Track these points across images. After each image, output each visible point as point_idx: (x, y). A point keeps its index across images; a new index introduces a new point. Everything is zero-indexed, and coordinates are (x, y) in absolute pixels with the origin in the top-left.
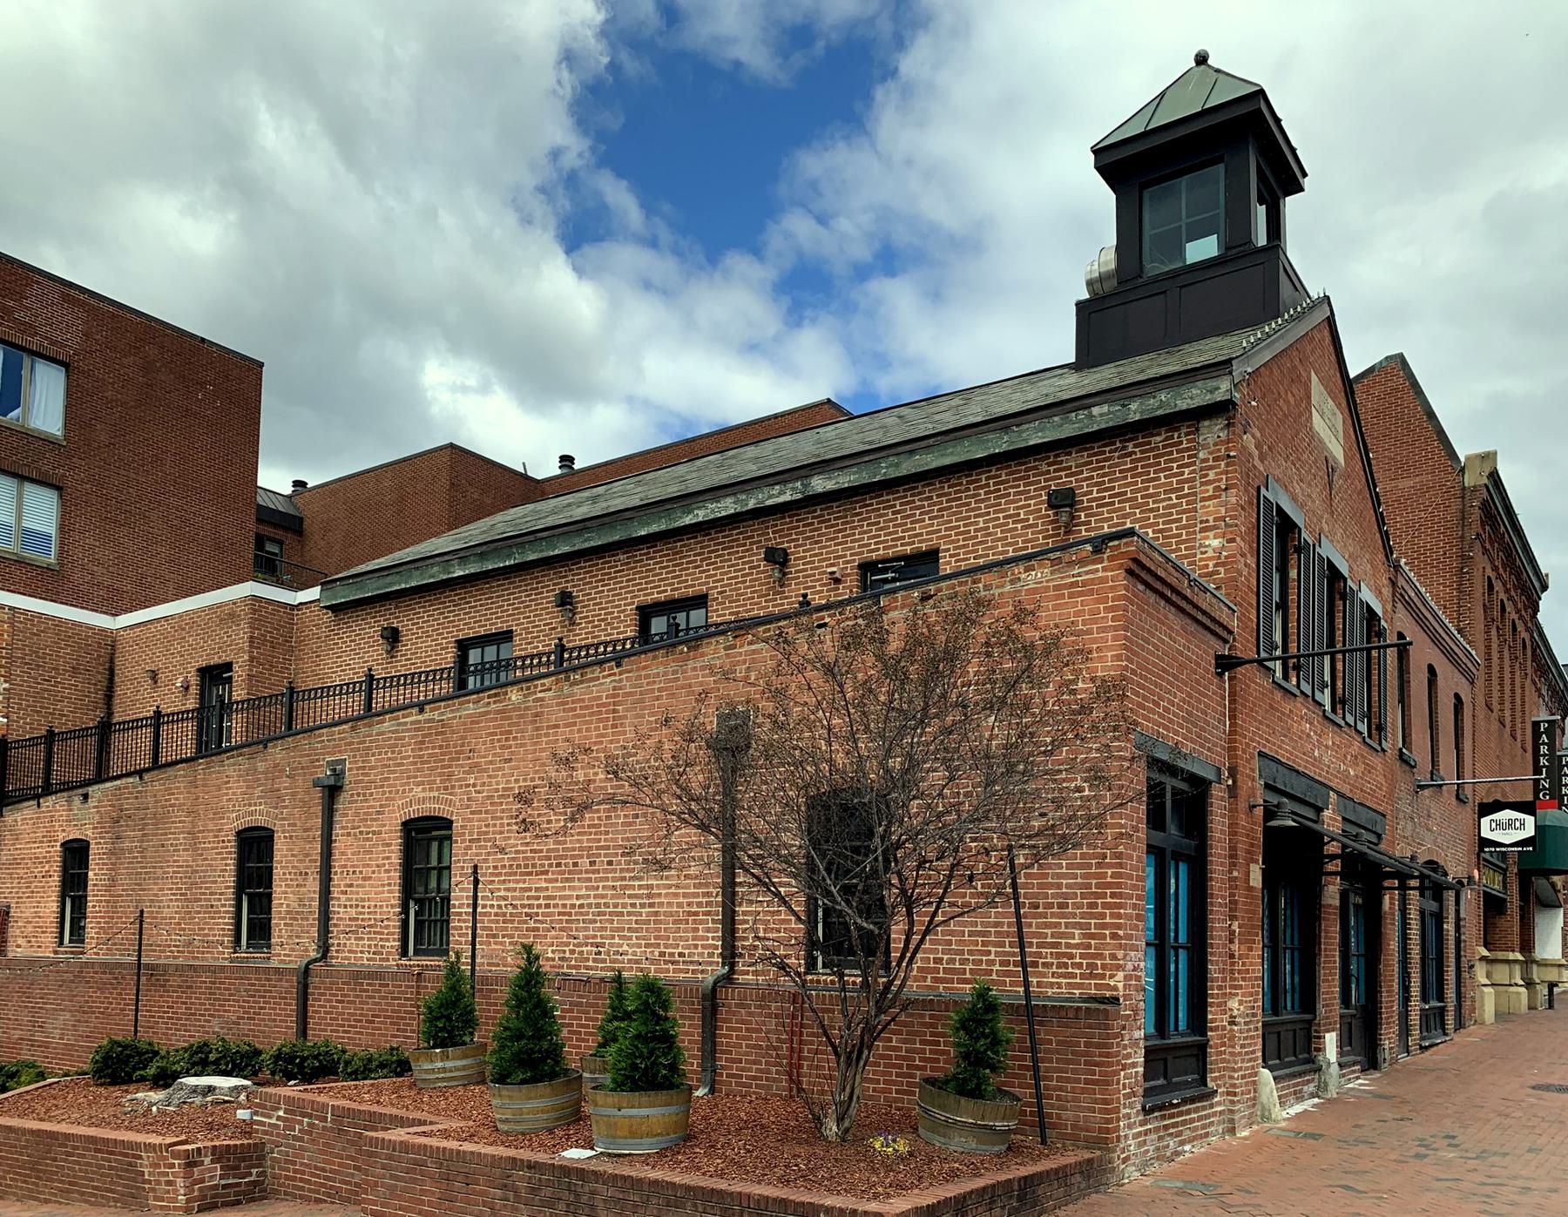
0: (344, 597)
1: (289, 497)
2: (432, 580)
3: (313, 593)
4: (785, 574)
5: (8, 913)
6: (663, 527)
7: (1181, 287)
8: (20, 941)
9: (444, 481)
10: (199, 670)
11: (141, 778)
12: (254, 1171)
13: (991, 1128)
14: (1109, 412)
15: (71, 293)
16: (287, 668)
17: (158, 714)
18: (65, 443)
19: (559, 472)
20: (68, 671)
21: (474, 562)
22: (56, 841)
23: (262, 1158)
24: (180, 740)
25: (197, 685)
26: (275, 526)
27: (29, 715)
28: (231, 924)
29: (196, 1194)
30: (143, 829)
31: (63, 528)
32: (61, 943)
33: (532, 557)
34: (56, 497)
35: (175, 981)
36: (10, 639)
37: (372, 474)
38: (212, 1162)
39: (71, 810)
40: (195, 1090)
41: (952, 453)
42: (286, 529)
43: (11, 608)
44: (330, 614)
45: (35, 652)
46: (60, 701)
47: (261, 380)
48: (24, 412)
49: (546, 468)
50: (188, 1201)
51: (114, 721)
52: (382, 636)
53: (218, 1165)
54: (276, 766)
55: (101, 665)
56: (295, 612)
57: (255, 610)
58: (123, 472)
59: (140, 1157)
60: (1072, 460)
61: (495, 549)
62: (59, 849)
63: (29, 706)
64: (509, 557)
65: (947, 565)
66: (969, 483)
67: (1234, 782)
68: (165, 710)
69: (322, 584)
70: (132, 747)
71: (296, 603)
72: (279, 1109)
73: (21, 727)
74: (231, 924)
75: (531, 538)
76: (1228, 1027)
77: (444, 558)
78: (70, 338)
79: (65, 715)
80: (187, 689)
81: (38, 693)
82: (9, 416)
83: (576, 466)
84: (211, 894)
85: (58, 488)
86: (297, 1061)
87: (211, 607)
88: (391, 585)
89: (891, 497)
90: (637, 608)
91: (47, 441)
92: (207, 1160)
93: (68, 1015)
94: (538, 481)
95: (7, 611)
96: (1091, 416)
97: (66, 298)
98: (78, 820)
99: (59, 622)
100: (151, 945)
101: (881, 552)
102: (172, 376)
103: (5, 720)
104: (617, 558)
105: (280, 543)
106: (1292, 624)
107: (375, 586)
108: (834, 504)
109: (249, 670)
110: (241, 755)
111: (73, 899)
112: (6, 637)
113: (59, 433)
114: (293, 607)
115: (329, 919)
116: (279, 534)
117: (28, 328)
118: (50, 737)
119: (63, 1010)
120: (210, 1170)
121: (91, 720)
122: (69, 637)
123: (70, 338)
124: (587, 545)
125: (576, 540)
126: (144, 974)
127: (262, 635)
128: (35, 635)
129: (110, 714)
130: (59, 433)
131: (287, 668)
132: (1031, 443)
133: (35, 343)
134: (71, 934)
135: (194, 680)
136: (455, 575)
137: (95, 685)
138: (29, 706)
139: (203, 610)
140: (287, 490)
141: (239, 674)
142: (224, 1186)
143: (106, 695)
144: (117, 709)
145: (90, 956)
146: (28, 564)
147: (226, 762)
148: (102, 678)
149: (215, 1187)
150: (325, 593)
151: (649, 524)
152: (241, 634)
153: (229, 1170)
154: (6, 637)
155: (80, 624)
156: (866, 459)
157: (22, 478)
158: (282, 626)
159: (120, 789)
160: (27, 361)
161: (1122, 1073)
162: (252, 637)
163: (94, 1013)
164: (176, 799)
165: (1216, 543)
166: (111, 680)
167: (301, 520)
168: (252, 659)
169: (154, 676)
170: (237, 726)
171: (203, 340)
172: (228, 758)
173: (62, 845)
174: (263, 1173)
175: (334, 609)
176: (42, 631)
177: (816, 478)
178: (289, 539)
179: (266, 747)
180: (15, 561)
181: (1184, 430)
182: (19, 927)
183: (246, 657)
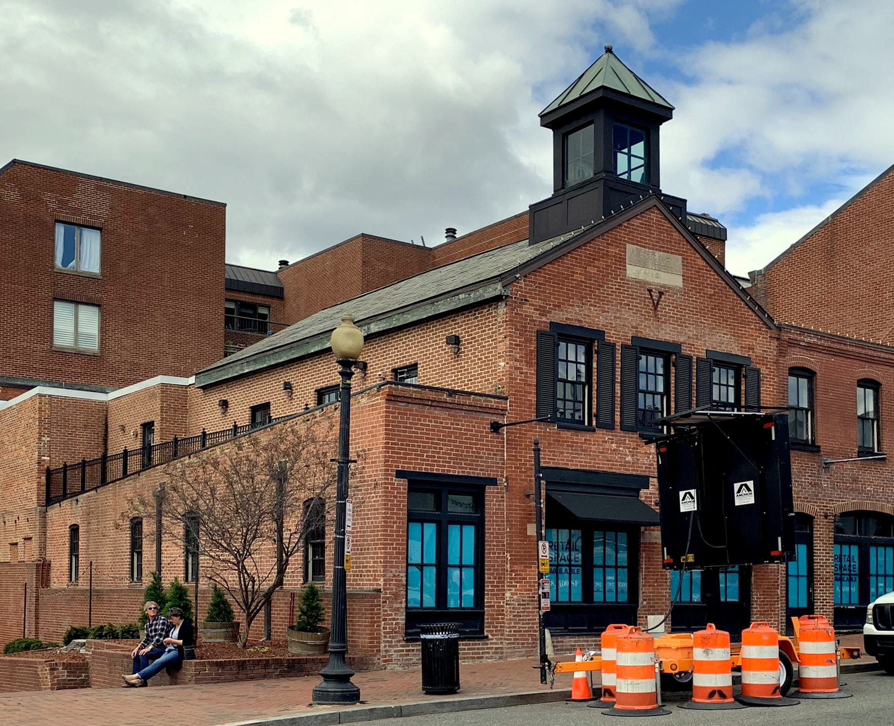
0: (203, 383)
1: (276, 273)
2: (237, 374)
3: (192, 380)
4: (365, 375)
5: (50, 565)
6: (320, 348)
7: (568, 200)
8: (55, 580)
9: (359, 261)
10: (142, 425)
11: (96, 491)
12: (83, 675)
13: (306, 643)
14: (465, 298)
15: (101, 184)
16: (184, 422)
17: (126, 451)
18: (101, 278)
19: (445, 240)
20: (81, 427)
21: (252, 365)
22: (67, 525)
23: (87, 669)
24: (134, 463)
25: (141, 433)
26: (264, 295)
27: (61, 454)
28: (129, 568)
29: (56, 682)
30: (98, 519)
31: (103, 330)
32: (71, 580)
33: (273, 363)
34: (97, 311)
35: (106, 598)
36: (49, 413)
37: (354, 241)
38: (63, 669)
39: (72, 508)
40: (78, 644)
41: (416, 315)
42: (272, 297)
43: (50, 396)
44: (202, 391)
45: (63, 419)
46: (78, 445)
47: (225, 215)
48: (77, 263)
49: (436, 240)
50: (52, 685)
51: (109, 455)
52: (220, 406)
53: (66, 671)
54: (143, 485)
55: (100, 422)
56: (188, 389)
57: (164, 391)
58: (137, 290)
59: (38, 668)
60: (460, 319)
61: (259, 358)
62: (68, 529)
63: (60, 449)
64: (265, 362)
65: (275, 413)
66: (427, 329)
67: (508, 484)
68: (68, 464)
69: (196, 374)
70: (115, 468)
71: (188, 384)
72: (91, 648)
73: (57, 461)
74: (129, 568)
75: (271, 352)
76: (505, 605)
77: (247, 360)
78: (101, 210)
79: (81, 453)
80: (137, 435)
81: (66, 441)
82: (69, 267)
83: (457, 236)
84: (122, 552)
85: (99, 306)
86: (131, 633)
87: (146, 389)
88: (221, 376)
89: (402, 335)
90: (316, 391)
91: (91, 278)
92: (60, 668)
93: (69, 618)
94: (431, 249)
95: (47, 397)
96: (459, 299)
97: (98, 188)
98: (75, 514)
99: (75, 401)
100: (102, 580)
101: (399, 364)
102: (166, 223)
103: (49, 458)
104: (307, 363)
105: (268, 307)
106: (594, 392)
107: (215, 376)
108: (383, 337)
109: (161, 425)
110: (131, 479)
111: (314, 545)
112: (47, 412)
113: (98, 272)
114: (187, 387)
115: (161, 564)
116: (267, 301)
117: (77, 211)
118: (84, 462)
119: (68, 615)
120: (62, 673)
121: (97, 454)
122: (82, 408)
123: (101, 210)
124: (293, 357)
125: (289, 354)
126: (92, 594)
127: (168, 405)
128: (63, 409)
129: (106, 450)
130: (98, 272)
131: (184, 422)
132: (441, 312)
133: (80, 219)
134: (313, 574)
135: (140, 431)
136: (245, 372)
137: (97, 434)
138: (60, 449)
139: (142, 391)
140: (274, 267)
141: (157, 427)
142: (69, 680)
143: (104, 439)
144: (109, 447)
145: (80, 587)
146: (83, 354)
147: (126, 483)
148: (101, 430)
149: (64, 680)
150: (198, 380)
151: (315, 346)
152: (157, 404)
153: (70, 673)
154: (47, 412)
155: (87, 400)
156: (388, 315)
157: (77, 303)
158: (180, 398)
159: (89, 497)
160: (77, 230)
161: (383, 622)
162: (162, 407)
163: (78, 616)
164: (109, 502)
165: (502, 364)
166: (106, 430)
167: (282, 289)
168: (162, 419)
169: (123, 428)
170: (156, 456)
171: (185, 196)
172: (127, 481)
173: (70, 527)
174: (88, 676)
175: (204, 388)
176: (67, 407)
177: (372, 324)
178: (275, 303)
179: (139, 475)
180: (75, 354)
181: (493, 307)
182: (55, 572)
183: (160, 419)
